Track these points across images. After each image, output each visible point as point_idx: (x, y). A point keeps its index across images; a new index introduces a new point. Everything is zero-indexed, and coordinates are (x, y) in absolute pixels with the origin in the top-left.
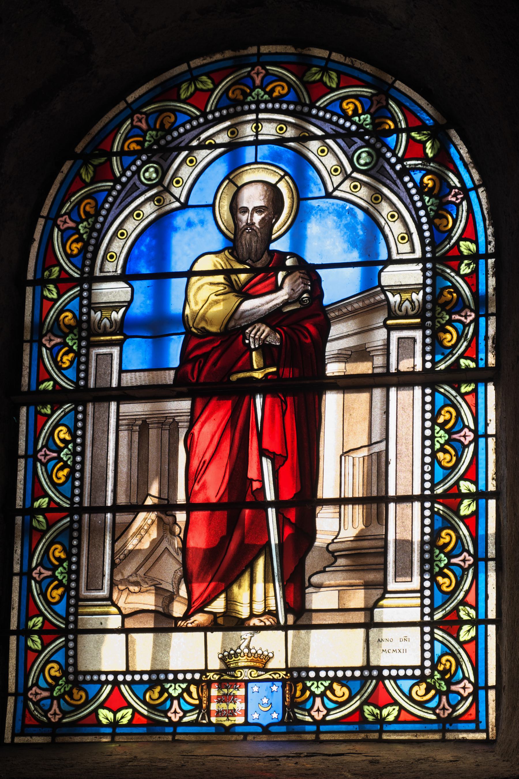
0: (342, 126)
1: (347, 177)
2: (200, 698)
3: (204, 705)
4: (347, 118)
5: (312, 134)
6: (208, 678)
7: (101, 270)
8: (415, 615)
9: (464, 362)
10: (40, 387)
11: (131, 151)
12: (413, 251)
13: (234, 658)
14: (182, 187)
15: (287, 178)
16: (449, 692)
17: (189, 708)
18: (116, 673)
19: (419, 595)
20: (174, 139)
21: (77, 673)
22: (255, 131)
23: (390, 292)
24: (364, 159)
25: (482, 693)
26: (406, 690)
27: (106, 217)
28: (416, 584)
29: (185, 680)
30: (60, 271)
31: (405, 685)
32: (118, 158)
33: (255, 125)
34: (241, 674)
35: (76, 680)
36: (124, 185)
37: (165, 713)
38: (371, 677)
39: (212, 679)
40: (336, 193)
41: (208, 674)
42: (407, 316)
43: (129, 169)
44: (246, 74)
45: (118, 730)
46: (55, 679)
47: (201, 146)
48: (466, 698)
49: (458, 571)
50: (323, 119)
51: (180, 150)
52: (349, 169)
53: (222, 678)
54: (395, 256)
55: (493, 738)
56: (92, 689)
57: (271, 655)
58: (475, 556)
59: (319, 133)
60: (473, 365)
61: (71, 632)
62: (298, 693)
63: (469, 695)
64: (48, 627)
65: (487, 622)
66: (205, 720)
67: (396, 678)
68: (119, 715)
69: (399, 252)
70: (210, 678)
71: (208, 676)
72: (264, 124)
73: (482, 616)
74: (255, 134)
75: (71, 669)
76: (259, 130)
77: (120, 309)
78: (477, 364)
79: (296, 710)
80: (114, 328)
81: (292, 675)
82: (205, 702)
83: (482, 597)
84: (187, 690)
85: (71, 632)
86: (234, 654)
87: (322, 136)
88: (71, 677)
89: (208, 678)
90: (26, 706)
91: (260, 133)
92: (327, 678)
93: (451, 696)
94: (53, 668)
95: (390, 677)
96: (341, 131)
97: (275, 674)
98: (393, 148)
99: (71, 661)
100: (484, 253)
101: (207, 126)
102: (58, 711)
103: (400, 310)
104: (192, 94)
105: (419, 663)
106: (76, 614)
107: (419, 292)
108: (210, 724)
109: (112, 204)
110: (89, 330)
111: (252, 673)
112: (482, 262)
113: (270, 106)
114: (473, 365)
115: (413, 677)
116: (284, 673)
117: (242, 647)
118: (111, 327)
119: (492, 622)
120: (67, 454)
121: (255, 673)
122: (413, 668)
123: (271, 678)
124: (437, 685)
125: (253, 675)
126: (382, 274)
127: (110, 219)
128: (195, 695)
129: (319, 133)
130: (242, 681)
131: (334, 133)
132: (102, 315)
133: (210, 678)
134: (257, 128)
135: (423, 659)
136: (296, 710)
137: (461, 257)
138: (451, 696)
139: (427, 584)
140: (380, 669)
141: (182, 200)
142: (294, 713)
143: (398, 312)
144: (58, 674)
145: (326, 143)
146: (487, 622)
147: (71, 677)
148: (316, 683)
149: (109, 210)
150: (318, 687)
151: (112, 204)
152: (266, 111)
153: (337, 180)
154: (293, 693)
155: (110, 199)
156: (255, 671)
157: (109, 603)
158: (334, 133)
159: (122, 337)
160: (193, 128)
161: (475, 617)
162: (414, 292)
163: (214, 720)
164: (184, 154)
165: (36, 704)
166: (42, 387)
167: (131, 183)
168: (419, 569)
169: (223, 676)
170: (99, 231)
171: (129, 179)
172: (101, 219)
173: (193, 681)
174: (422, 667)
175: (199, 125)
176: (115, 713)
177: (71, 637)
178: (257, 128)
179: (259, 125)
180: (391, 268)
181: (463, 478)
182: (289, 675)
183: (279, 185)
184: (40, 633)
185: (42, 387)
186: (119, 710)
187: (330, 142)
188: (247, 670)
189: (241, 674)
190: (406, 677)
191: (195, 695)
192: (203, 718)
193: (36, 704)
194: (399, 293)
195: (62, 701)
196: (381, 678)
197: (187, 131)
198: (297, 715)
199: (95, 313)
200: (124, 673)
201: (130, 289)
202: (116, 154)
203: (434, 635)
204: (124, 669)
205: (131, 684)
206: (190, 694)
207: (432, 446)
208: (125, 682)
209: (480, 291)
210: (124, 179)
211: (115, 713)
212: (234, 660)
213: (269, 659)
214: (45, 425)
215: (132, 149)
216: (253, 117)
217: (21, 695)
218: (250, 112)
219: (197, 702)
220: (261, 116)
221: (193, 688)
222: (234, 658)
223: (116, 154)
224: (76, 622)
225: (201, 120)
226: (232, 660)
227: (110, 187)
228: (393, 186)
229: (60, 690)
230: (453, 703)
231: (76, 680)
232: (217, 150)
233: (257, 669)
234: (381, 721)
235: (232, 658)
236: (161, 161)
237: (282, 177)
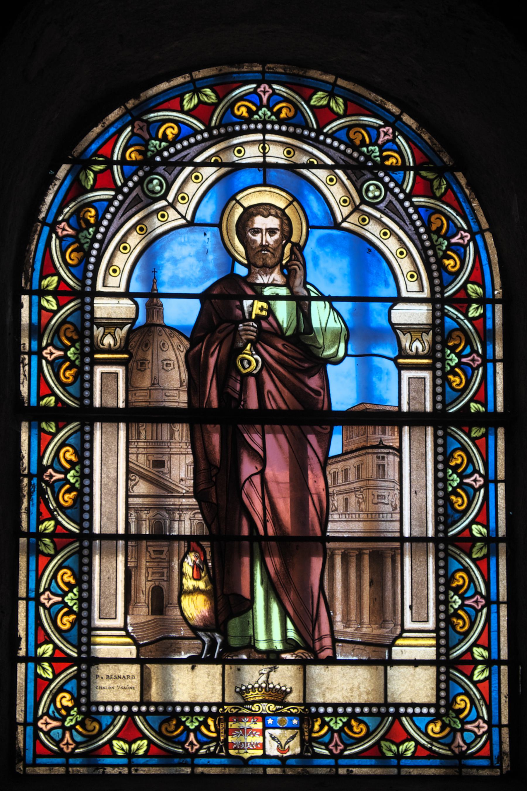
0: (350, 156)
1: (356, 209)
2: (217, 731)
3: (222, 738)
4: (356, 148)
5: (322, 163)
6: (226, 711)
7: (104, 285)
8: (430, 654)
9: (474, 407)
10: (41, 403)
11: (133, 161)
12: (422, 291)
13: (251, 693)
14: (188, 203)
15: (295, 203)
16: (463, 730)
17: (205, 739)
18: (130, 704)
19: (434, 635)
20: (177, 152)
21: (89, 704)
22: (262, 151)
23: (400, 330)
24: (372, 192)
25: (495, 731)
26: (67, 687)
27: (107, 228)
28: (431, 625)
29: (201, 713)
30: (59, 282)
31: (421, 722)
32: (119, 167)
33: (262, 145)
34: (259, 708)
35: (89, 711)
36: (126, 196)
37: (182, 744)
38: (388, 714)
39: (229, 712)
40: (345, 225)
41: (225, 707)
42: (417, 356)
43: (131, 179)
44: (481, 715)
45: (135, 761)
46: (68, 709)
47: (205, 164)
48: (481, 736)
49: (472, 612)
50: (331, 146)
51: (184, 165)
52: (358, 201)
53: (240, 712)
54: (404, 294)
55: (188, 77)
56: (106, 720)
57: (288, 690)
58: (485, 477)
59: (329, 162)
60: (482, 409)
61: (84, 661)
62: (317, 727)
63: (484, 733)
64: (59, 654)
65: (500, 662)
66: (223, 752)
67: (411, 716)
68: (134, 746)
69: (409, 290)
70: (228, 711)
71: (225, 709)
72: (271, 146)
73: (494, 656)
74: (262, 155)
75: (83, 700)
76: (267, 151)
77: (124, 327)
78: (486, 408)
79: (314, 744)
80: (118, 344)
81: (310, 710)
82: (223, 734)
83: (494, 635)
84: (205, 723)
85: (84, 661)
86: (258, 688)
87: (332, 165)
88: (84, 709)
89: (226, 711)
90: (36, 737)
91: (267, 155)
92: (345, 714)
93: (60, 731)
94: (64, 697)
95: (406, 714)
96: (351, 162)
97: (294, 708)
98: (400, 183)
99: (83, 692)
100: (493, 411)
101: (211, 142)
102: (70, 742)
103: (411, 350)
104: (195, 107)
105: (434, 700)
106: (89, 644)
107: (429, 332)
108: (228, 756)
109: (114, 215)
110: (91, 345)
111: (271, 707)
112: (489, 307)
113: (276, 127)
114: (482, 409)
115: (428, 714)
116: (303, 708)
117: (260, 682)
118: (115, 345)
119: (504, 663)
120: (74, 476)
121: (273, 707)
122: (428, 706)
123: (289, 712)
124: (452, 723)
125: (271, 709)
126: (392, 311)
127: (112, 230)
128: (212, 728)
129: (329, 162)
130: (260, 715)
131: (343, 163)
132: (104, 332)
133: (228, 711)
134: (264, 148)
135: (438, 697)
136: (314, 744)
137: (469, 301)
138: (60, 731)
139: (442, 625)
140: (397, 706)
141: (189, 217)
142: (312, 747)
143: (409, 351)
144: (70, 704)
145: (335, 173)
146: (500, 662)
147: (84, 709)
148: (334, 719)
149: (111, 221)
150: (336, 722)
151: (114, 215)
152: (273, 132)
153: (346, 211)
154: (310, 727)
155: (112, 209)
156: (273, 705)
157: (123, 633)
158: (343, 163)
159: (126, 356)
160: (197, 143)
161: (486, 535)
162: (424, 332)
163: (232, 752)
164: (188, 169)
165: (47, 733)
166: (43, 403)
167: (134, 194)
168: (435, 608)
169: (240, 709)
170: (101, 242)
171: (131, 190)
172: (102, 230)
173: (210, 714)
174: (437, 706)
175: (204, 140)
176: (130, 745)
177: (84, 667)
178: (264, 148)
179: (266, 145)
180: (400, 306)
181: (474, 522)
182: (307, 710)
183: (287, 211)
184: (51, 660)
185: (43, 403)
186: (135, 741)
187: (339, 172)
188: (265, 704)
189: (259, 708)
190: (421, 714)
191: (212, 728)
192: (221, 750)
193: (47, 733)
194: (409, 332)
195: (74, 733)
196: (397, 716)
197: (191, 145)
198: (315, 748)
199: (98, 328)
200: (139, 704)
201: (134, 306)
202: (117, 163)
203: (449, 675)
204: (138, 699)
205: (144, 715)
206: (208, 727)
207: (445, 489)
208: (139, 713)
209: (488, 356)
210: (126, 190)
211: (130, 745)
212: (252, 695)
213: (286, 693)
214: (49, 444)
215: (134, 159)
216: (259, 137)
217: (30, 724)
218: (256, 131)
219: (214, 735)
220: (268, 137)
221: (210, 722)
222: (251, 693)
223: (117, 163)
224: (89, 652)
225: (206, 135)
226: (256, 693)
227: (112, 197)
228: (402, 223)
229: (71, 720)
230: (468, 741)
231: (89, 711)
232: (223, 168)
233: (276, 703)
234: (399, 756)
235: (255, 692)
236: (166, 174)
237: (291, 203)
